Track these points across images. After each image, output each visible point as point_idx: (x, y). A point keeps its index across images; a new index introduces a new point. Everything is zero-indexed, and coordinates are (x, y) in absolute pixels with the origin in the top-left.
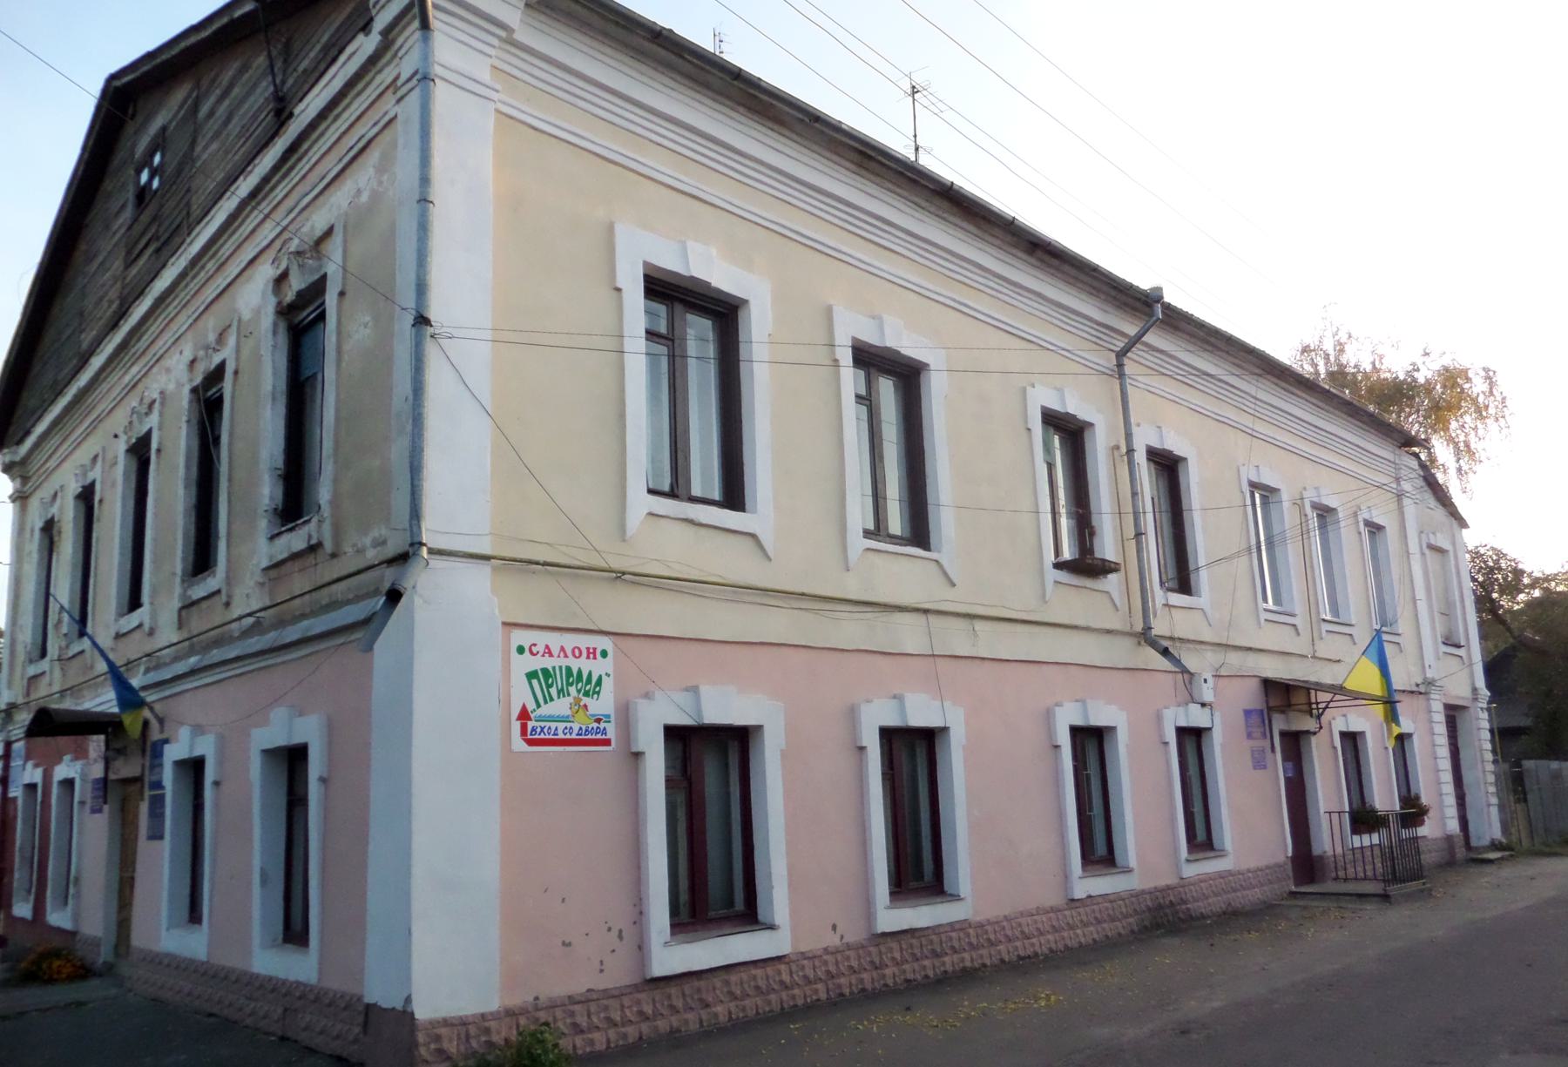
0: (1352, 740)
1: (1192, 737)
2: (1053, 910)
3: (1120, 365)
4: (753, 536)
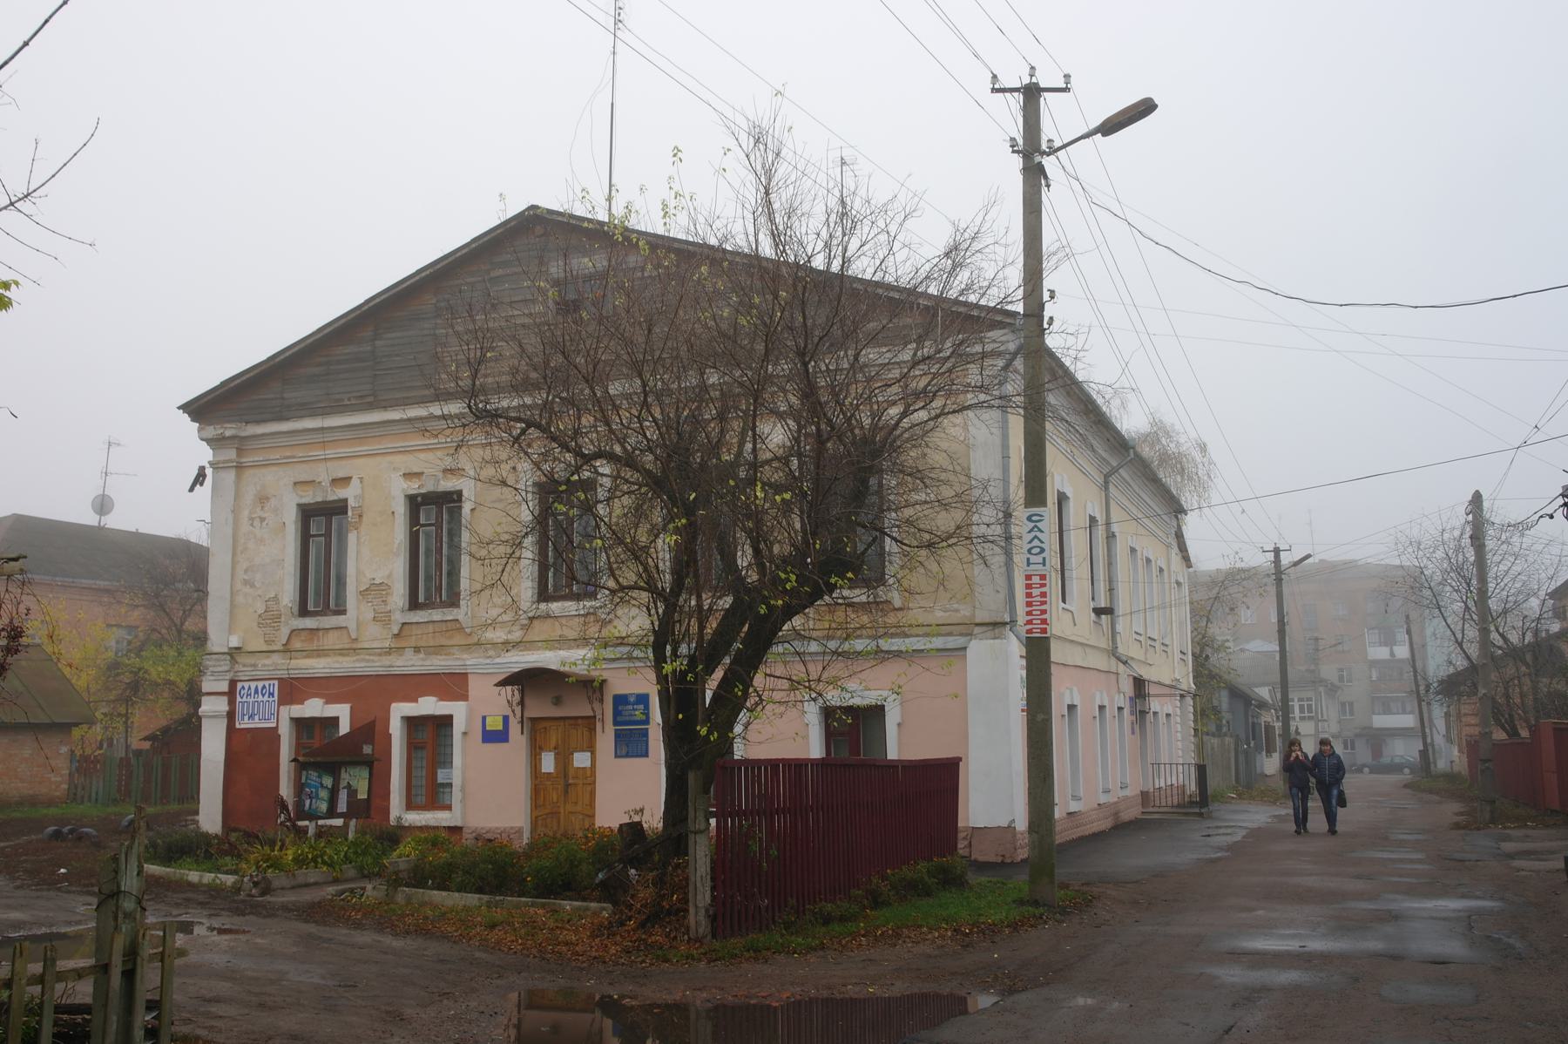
0: (1155, 713)
1: (1120, 709)
2: (1095, 810)
3: (1106, 482)
4: (1072, 612)
